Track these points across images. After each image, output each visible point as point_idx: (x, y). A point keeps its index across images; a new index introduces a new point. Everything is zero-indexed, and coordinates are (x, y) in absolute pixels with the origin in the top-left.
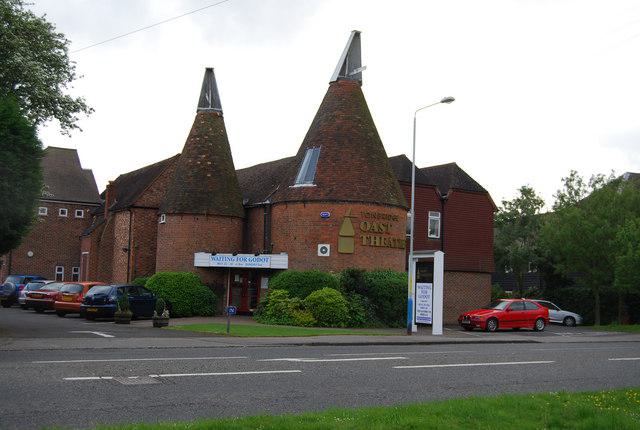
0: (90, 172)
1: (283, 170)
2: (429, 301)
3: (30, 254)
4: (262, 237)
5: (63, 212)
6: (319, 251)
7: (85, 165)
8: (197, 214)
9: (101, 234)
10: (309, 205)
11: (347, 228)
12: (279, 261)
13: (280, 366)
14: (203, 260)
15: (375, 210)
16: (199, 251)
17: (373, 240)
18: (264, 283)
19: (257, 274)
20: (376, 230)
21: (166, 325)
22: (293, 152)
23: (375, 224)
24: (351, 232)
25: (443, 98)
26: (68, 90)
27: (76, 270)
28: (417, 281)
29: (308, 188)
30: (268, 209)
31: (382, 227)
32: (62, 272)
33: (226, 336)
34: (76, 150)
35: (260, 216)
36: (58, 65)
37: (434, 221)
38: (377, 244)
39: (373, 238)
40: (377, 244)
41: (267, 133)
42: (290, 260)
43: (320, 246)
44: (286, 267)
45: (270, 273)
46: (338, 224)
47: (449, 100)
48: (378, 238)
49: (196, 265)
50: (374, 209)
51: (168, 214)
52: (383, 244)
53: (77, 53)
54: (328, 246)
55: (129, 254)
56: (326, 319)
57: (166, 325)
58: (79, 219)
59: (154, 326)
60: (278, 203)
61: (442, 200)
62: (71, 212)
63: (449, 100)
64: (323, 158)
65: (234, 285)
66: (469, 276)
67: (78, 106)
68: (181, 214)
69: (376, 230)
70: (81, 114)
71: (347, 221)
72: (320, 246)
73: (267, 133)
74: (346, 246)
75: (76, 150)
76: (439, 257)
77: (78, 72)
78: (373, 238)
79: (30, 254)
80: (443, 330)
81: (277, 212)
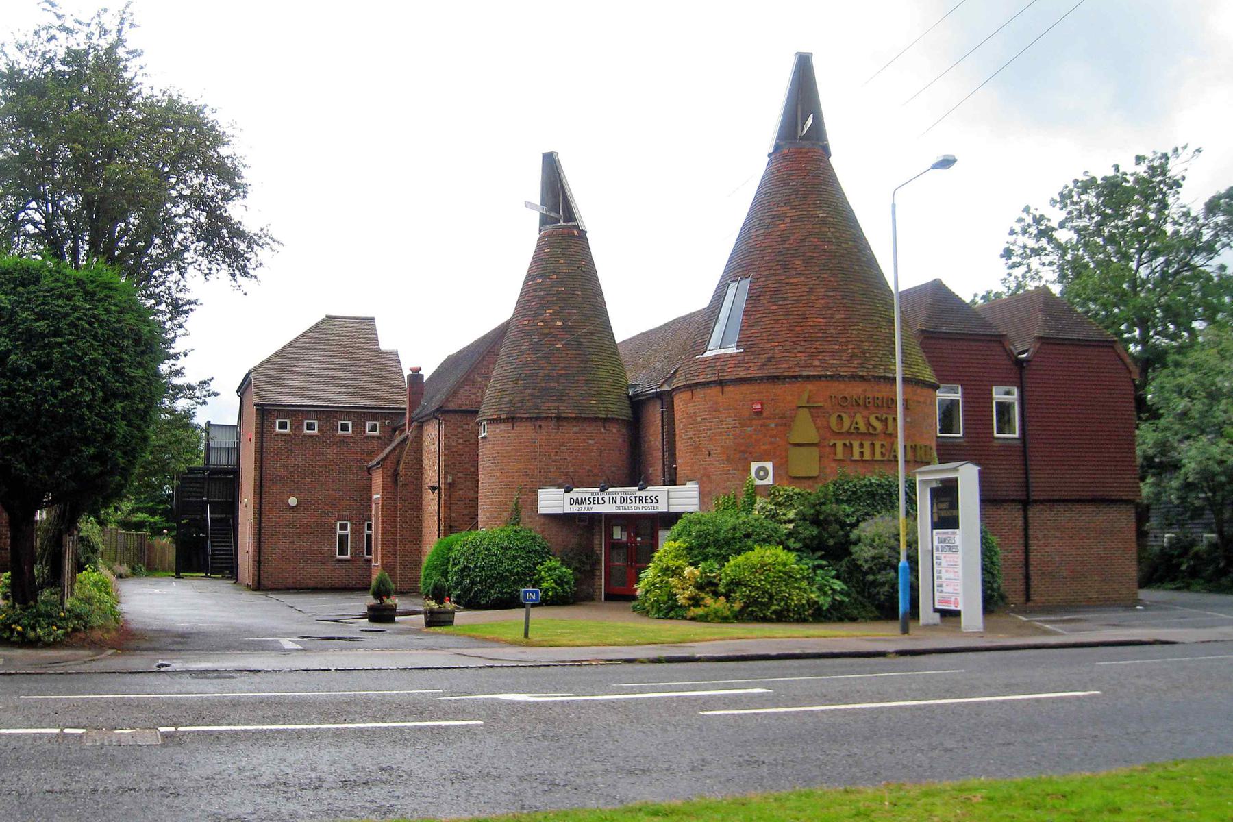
0: (395, 354)
1: (694, 329)
2: (952, 569)
4: (659, 454)
5: (345, 427)
6: (753, 475)
7: (385, 344)
8: (537, 419)
9: (398, 463)
10: (730, 390)
11: (804, 429)
12: (683, 498)
14: (553, 501)
15: (860, 390)
16: (543, 486)
17: (856, 450)
20: (863, 428)
21: (450, 622)
22: (701, 301)
23: (859, 418)
24: (813, 436)
25: (935, 161)
27: (343, 527)
28: (236, 472)
29: (732, 356)
32: (348, 531)
33: (520, 644)
34: (373, 319)
35: (655, 414)
38: (867, 456)
39: (856, 444)
40: (867, 456)
41: (666, 273)
42: (703, 495)
43: (754, 466)
45: (669, 519)
46: (786, 422)
47: (946, 163)
48: (867, 444)
49: (542, 510)
50: (855, 390)
51: (491, 421)
52: (878, 456)
54: (769, 465)
55: (439, 494)
56: (759, 608)
57: (450, 622)
58: (373, 437)
59: (429, 624)
61: (1020, 364)
63: (946, 163)
64: (754, 299)
65: (612, 546)
66: (1089, 509)
68: (512, 419)
71: (804, 414)
72: (754, 466)
73: (666, 273)
74: (805, 463)
75: (373, 319)
76: (968, 477)
77: (247, 176)
78: (856, 444)
79: (293, 501)
80: (984, 623)
81: (680, 403)
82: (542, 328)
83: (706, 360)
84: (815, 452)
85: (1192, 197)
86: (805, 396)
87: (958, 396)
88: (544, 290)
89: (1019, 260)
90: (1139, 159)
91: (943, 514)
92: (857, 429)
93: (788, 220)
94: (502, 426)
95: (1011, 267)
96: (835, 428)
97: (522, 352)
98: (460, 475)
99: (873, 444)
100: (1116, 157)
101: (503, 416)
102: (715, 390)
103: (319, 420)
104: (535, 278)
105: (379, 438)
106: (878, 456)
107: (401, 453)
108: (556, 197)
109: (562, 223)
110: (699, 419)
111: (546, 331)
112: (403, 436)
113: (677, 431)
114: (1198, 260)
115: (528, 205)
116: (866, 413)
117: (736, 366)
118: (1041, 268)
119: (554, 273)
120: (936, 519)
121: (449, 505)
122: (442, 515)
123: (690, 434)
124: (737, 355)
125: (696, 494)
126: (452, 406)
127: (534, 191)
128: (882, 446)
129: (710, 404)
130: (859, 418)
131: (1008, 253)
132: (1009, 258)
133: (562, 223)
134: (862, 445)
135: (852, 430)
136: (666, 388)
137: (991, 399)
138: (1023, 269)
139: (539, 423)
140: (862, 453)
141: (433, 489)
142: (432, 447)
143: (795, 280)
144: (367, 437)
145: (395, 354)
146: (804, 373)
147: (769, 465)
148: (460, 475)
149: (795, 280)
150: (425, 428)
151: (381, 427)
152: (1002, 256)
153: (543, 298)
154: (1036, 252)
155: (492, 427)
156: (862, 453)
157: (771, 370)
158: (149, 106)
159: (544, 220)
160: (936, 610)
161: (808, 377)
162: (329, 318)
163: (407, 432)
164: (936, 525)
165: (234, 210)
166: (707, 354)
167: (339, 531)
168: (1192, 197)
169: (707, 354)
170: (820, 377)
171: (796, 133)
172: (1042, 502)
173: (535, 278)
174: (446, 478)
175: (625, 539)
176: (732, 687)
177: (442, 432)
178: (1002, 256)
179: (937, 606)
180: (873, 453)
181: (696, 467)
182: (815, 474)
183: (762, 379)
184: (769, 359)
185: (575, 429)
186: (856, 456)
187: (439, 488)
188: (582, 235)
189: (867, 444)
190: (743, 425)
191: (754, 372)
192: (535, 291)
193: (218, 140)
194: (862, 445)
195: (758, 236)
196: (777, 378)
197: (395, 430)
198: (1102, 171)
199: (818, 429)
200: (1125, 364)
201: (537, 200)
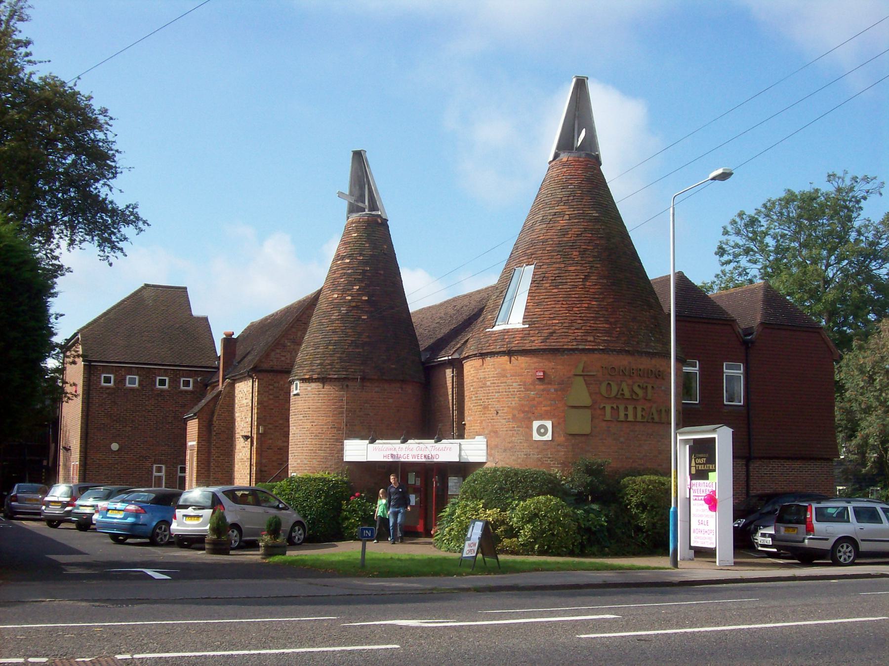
2: (703, 518)
3: (115, 446)
12: (473, 449)
13: (598, 568)
14: (357, 450)
18: (452, 481)
19: (444, 470)
20: (627, 394)
22: (492, 280)
26: (117, 192)
27: (159, 470)
30: (457, 365)
31: (636, 389)
32: (163, 474)
34: (186, 288)
36: (101, 160)
37: (730, 378)
38: (631, 418)
39: (622, 408)
43: (536, 424)
44: (483, 459)
45: (462, 469)
48: (630, 408)
51: (304, 380)
53: (123, 135)
58: (186, 392)
60: (468, 357)
61: (746, 344)
62: (174, 382)
63: (724, 176)
66: (796, 464)
67: (129, 217)
69: (627, 394)
70: (127, 230)
72: (536, 424)
75: (186, 288)
76: (723, 438)
77: (121, 161)
78: (622, 408)
81: (469, 368)
82: (350, 301)
83: (493, 333)
84: (588, 413)
85: (871, 212)
86: (581, 366)
87: (695, 370)
88: (352, 268)
89: (731, 257)
90: (831, 177)
91: (701, 467)
92: (623, 394)
93: (567, 217)
94: (313, 385)
95: (723, 264)
96: (604, 392)
97: (333, 322)
98: (270, 426)
99: (635, 408)
100: (811, 178)
101: (315, 376)
102: (506, 358)
103: (140, 376)
104: (343, 258)
105: (192, 392)
106: (639, 418)
107: (215, 405)
108: (362, 188)
109: (367, 212)
110: (488, 383)
111: (354, 304)
112: (215, 392)
113: (466, 393)
114: (873, 265)
115: (341, 195)
116: (630, 382)
117: (523, 338)
118: (749, 265)
119: (361, 255)
120: (693, 472)
121: (260, 453)
122: (254, 461)
123: (480, 396)
124: (523, 330)
125: (485, 447)
126: (265, 366)
127: (344, 182)
128: (643, 409)
129: (499, 370)
130: (624, 386)
131: (721, 251)
132: (722, 255)
133: (367, 212)
134: (626, 409)
135: (619, 396)
136: (456, 356)
137: (723, 372)
138: (733, 265)
139: (346, 383)
140: (626, 415)
141: (246, 438)
142: (245, 401)
143: (573, 268)
144: (182, 392)
145: (206, 319)
146: (580, 347)
147: (549, 424)
148: (270, 426)
149: (573, 268)
150: (237, 385)
151: (194, 383)
152: (716, 254)
153: (349, 275)
154: (747, 251)
155: (305, 385)
156: (626, 415)
157: (552, 344)
158: (27, 90)
159: (352, 209)
160: (691, 548)
161: (583, 350)
162: (147, 285)
163: (221, 387)
164: (693, 477)
165: (101, 189)
166: (496, 328)
167: (155, 474)
168: (871, 212)
169: (496, 328)
170: (593, 350)
171: (573, 144)
172: (760, 458)
173: (343, 258)
174: (258, 429)
175: (418, 483)
176: (551, 614)
177: (256, 389)
178: (716, 254)
179: (692, 544)
180: (635, 416)
181: (484, 424)
182: (587, 430)
183: (544, 350)
184: (551, 334)
185: (377, 389)
186: (622, 417)
187: (252, 438)
188: (384, 223)
189: (630, 408)
190: (527, 390)
191: (537, 344)
192: (343, 269)
193: (94, 124)
194: (626, 409)
195: (542, 229)
196: (558, 350)
197: (207, 386)
198: (801, 187)
199: (591, 394)
200: (828, 347)
201: (347, 192)
